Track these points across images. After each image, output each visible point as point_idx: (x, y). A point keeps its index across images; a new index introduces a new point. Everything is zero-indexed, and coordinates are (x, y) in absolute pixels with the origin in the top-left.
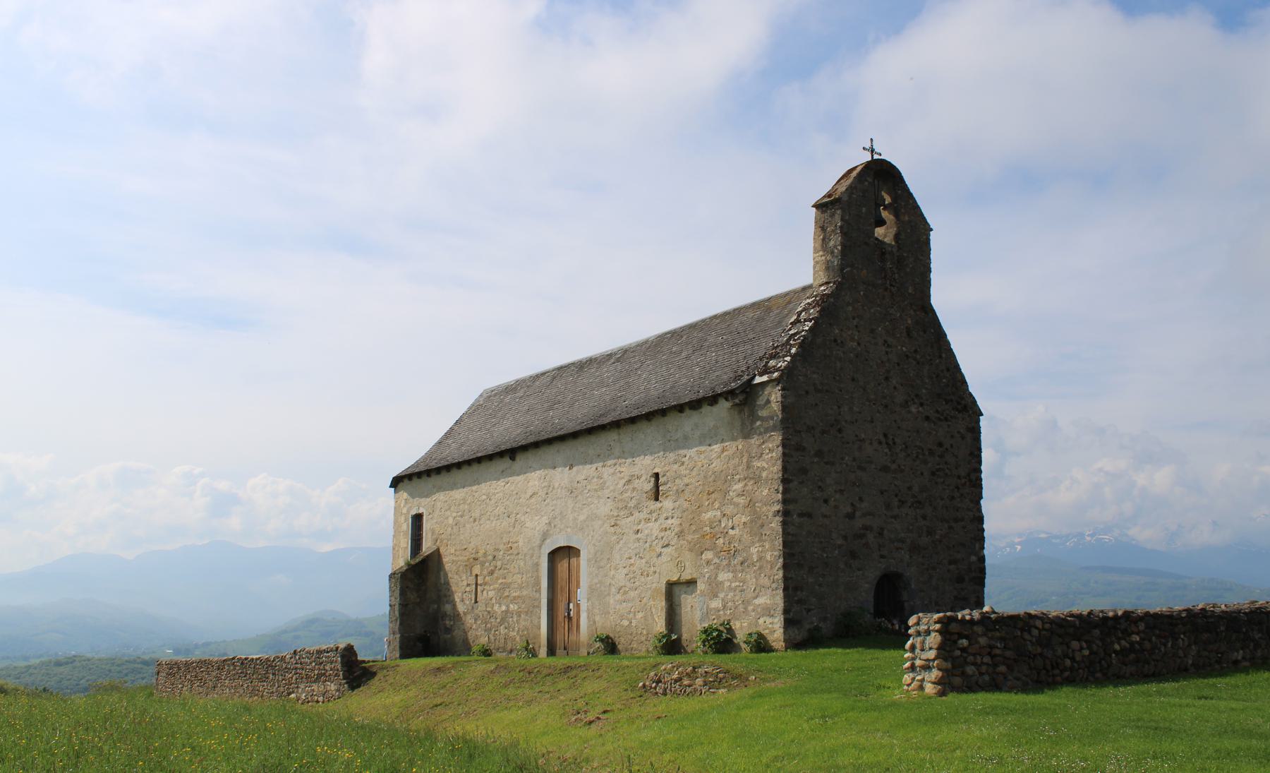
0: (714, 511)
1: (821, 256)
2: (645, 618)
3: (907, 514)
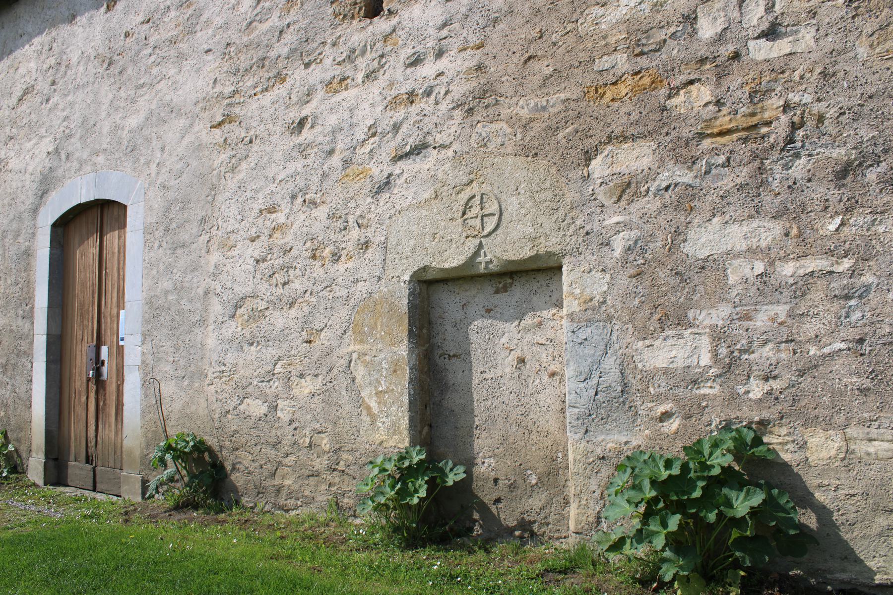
2: (326, 395)
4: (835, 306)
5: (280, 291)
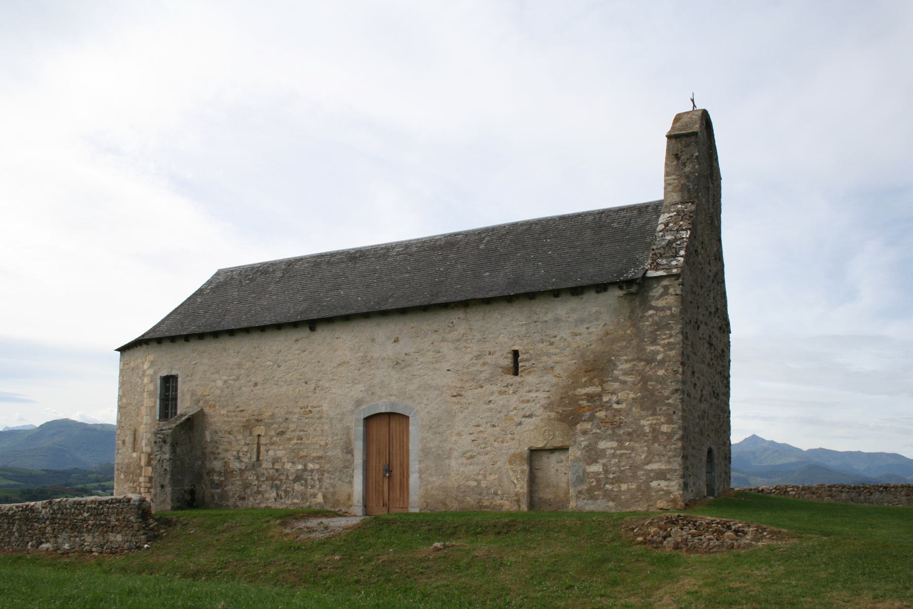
5: (482, 450)
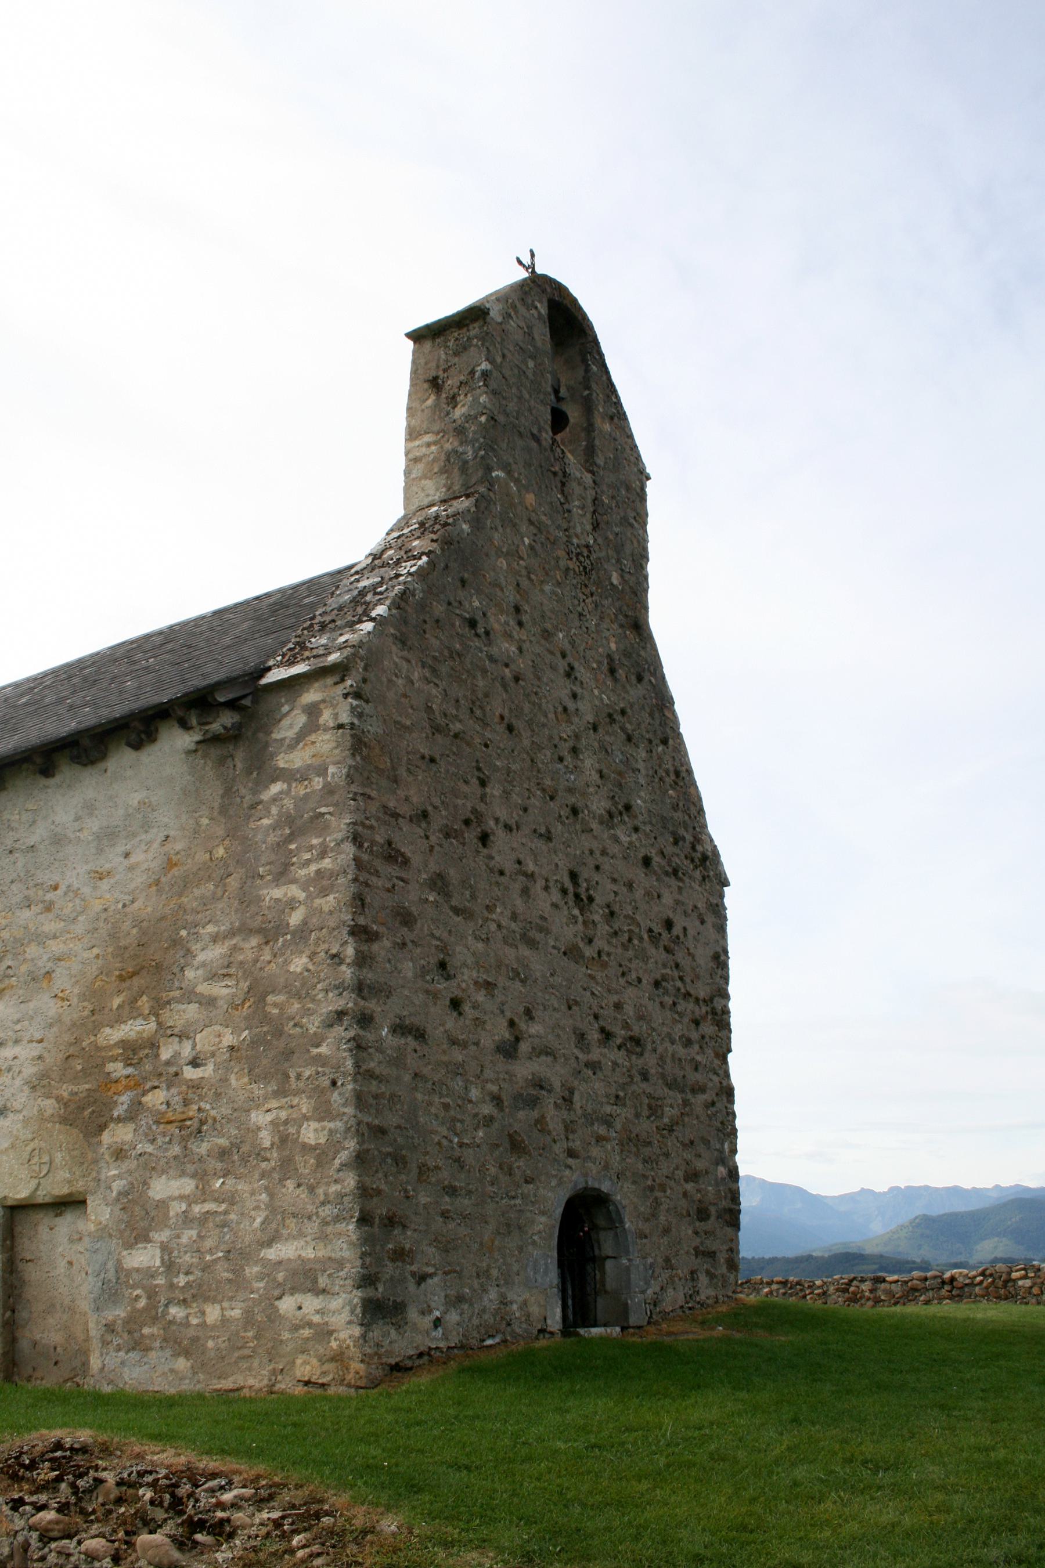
0: (140, 1021)
1: (429, 445)
3: (615, 1064)
4: (218, 1230)
